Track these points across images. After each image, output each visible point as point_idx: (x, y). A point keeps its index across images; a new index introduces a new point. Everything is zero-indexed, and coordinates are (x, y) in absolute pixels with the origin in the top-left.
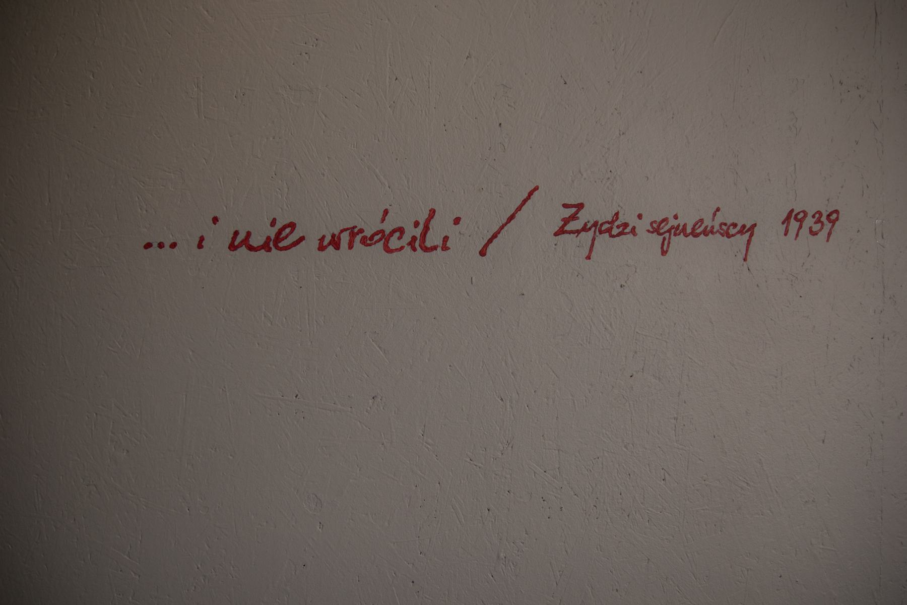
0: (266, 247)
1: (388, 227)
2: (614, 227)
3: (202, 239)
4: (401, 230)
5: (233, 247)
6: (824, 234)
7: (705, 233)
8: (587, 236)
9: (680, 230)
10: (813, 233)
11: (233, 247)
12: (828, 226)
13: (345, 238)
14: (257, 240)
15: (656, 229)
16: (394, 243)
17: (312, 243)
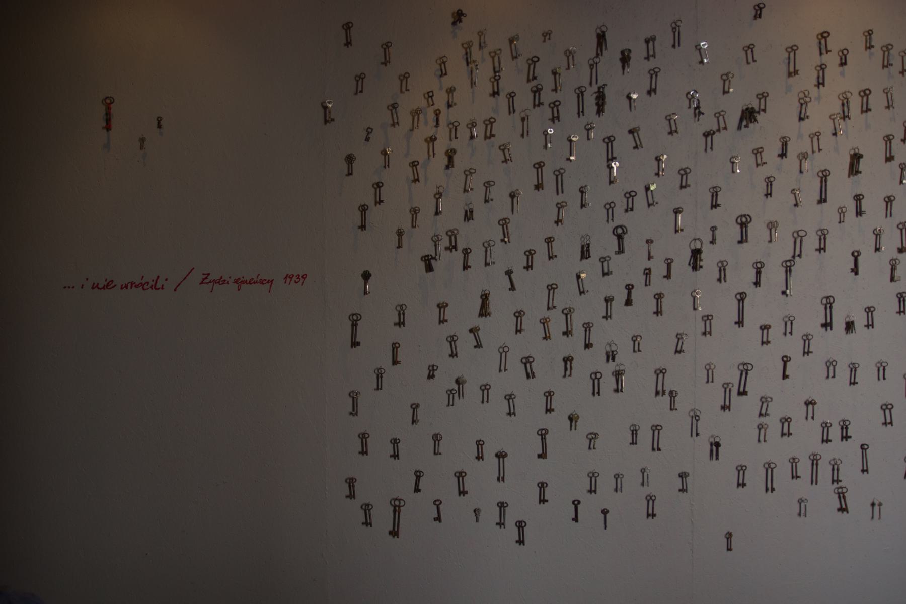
0: (104, 288)
1: (144, 282)
2: (221, 281)
3: (159, 120)
4: (148, 283)
5: (93, 288)
6: (300, 283)
7: (254, 283)
8: (211, 285)
9: (245, 282)
10: (296, 282)
11: (93, 288)
12: (302, 280)
13: (129, 285)
14: (101, 286)
15: (236, 282)
16: (146, 287)
17: (119, 286)
